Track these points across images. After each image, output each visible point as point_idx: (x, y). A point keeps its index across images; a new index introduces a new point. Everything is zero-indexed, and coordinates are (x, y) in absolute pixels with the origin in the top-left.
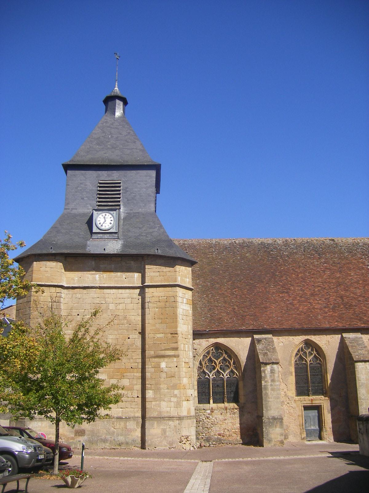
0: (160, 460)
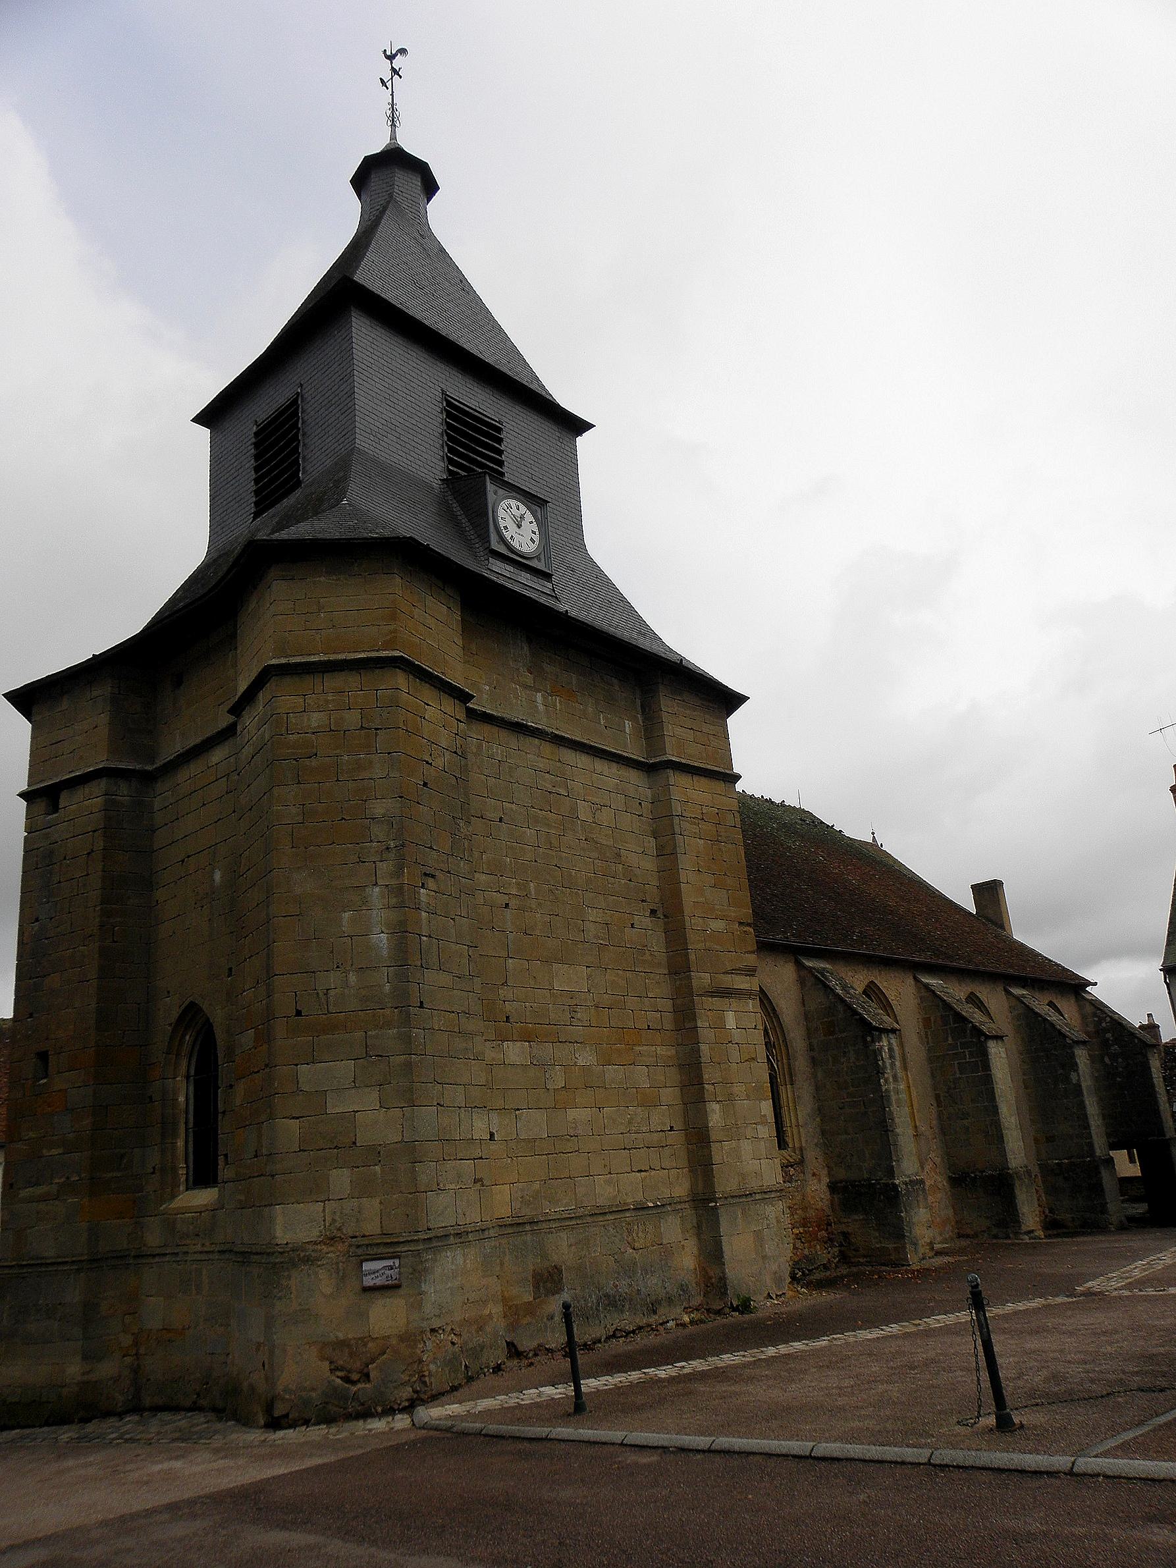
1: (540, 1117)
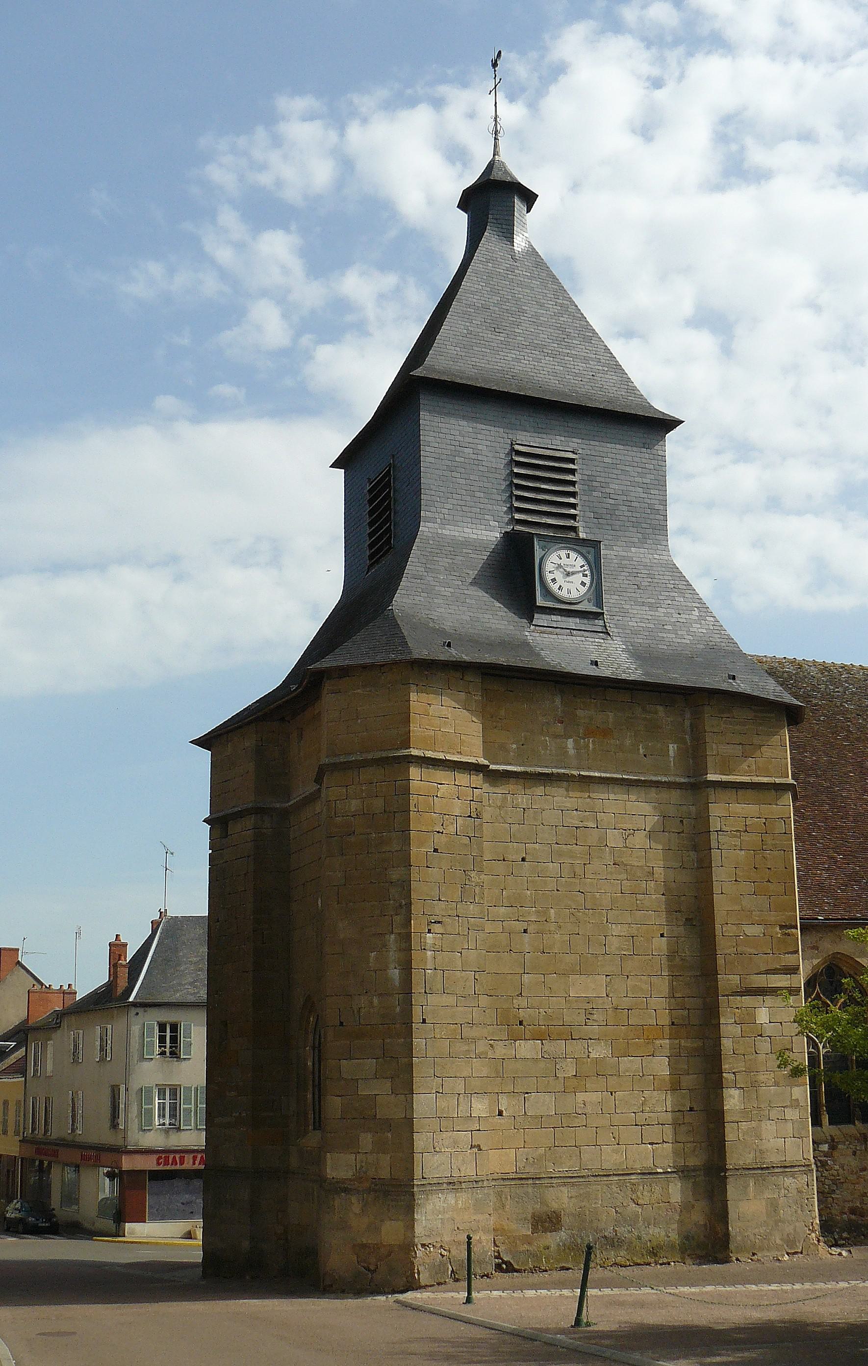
0: (558, 1294)
1: (549, 1099)
